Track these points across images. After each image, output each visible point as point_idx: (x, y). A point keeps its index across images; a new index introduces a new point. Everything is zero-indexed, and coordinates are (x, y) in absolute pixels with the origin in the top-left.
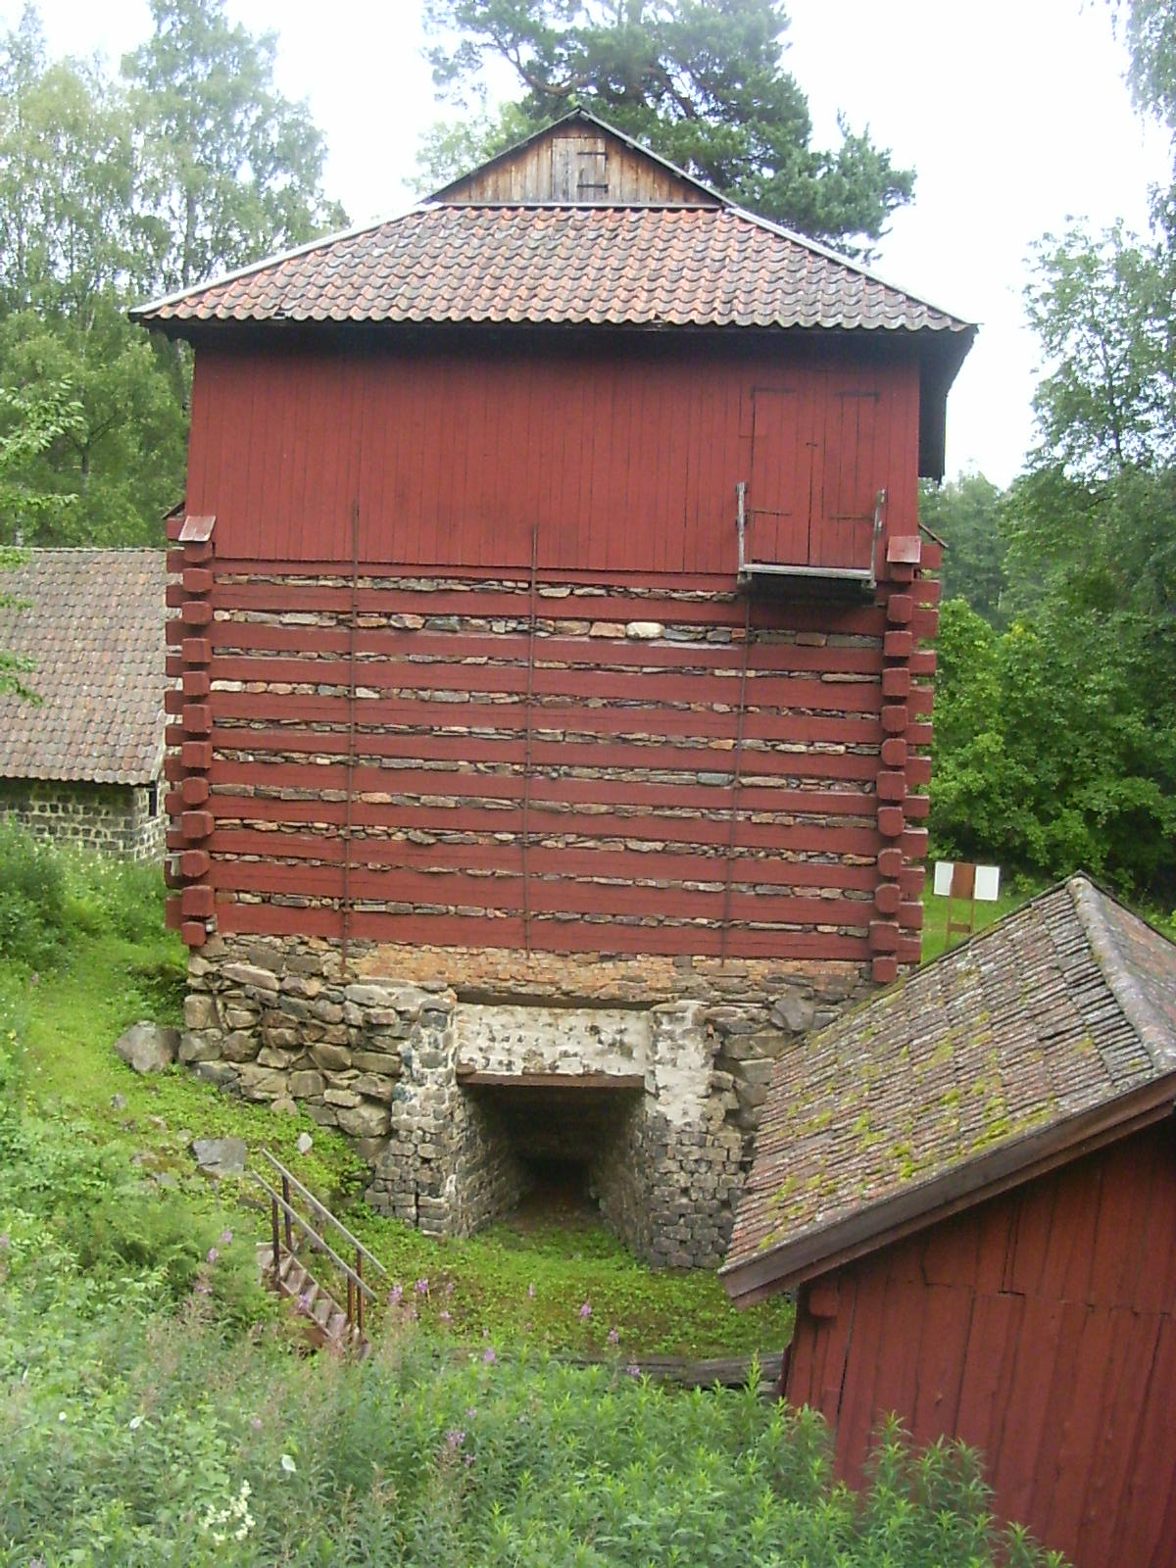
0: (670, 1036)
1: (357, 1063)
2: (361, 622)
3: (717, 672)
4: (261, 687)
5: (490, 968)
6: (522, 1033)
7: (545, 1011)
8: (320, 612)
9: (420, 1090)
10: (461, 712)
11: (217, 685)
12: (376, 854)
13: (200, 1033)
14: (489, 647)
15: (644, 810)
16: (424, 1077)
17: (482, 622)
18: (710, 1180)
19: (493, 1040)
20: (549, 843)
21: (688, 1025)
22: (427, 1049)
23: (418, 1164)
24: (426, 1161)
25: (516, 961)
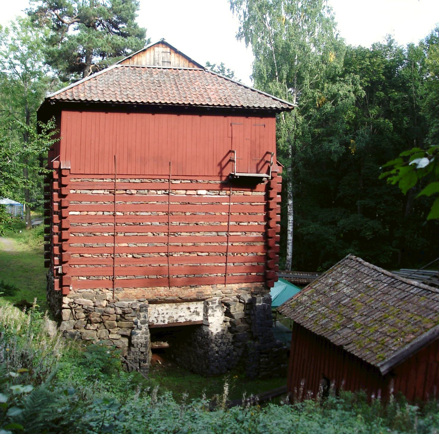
0: (212, 308)
1: (119, 325)
2: (117, 192)
3: (223, 204)
4: (85, 213)
5: (158, 293)
6: (168, 311)
7: (174, 304)
8: (104, 190)
9: (141, 331)
10: (149, 218)
11: (71, 213)
12: (123, 262)
13: (417, 334)
14: (157, 199)
15: (202, 244)
16: (141, 327)
17: (154, 191)
18: (224, 348)
19: (159, 314)
20: (176, 255)
21: (217, 304)
22: (142, 319)
23: (140, 354)
24: (142, 353)
25: (166, 291)
